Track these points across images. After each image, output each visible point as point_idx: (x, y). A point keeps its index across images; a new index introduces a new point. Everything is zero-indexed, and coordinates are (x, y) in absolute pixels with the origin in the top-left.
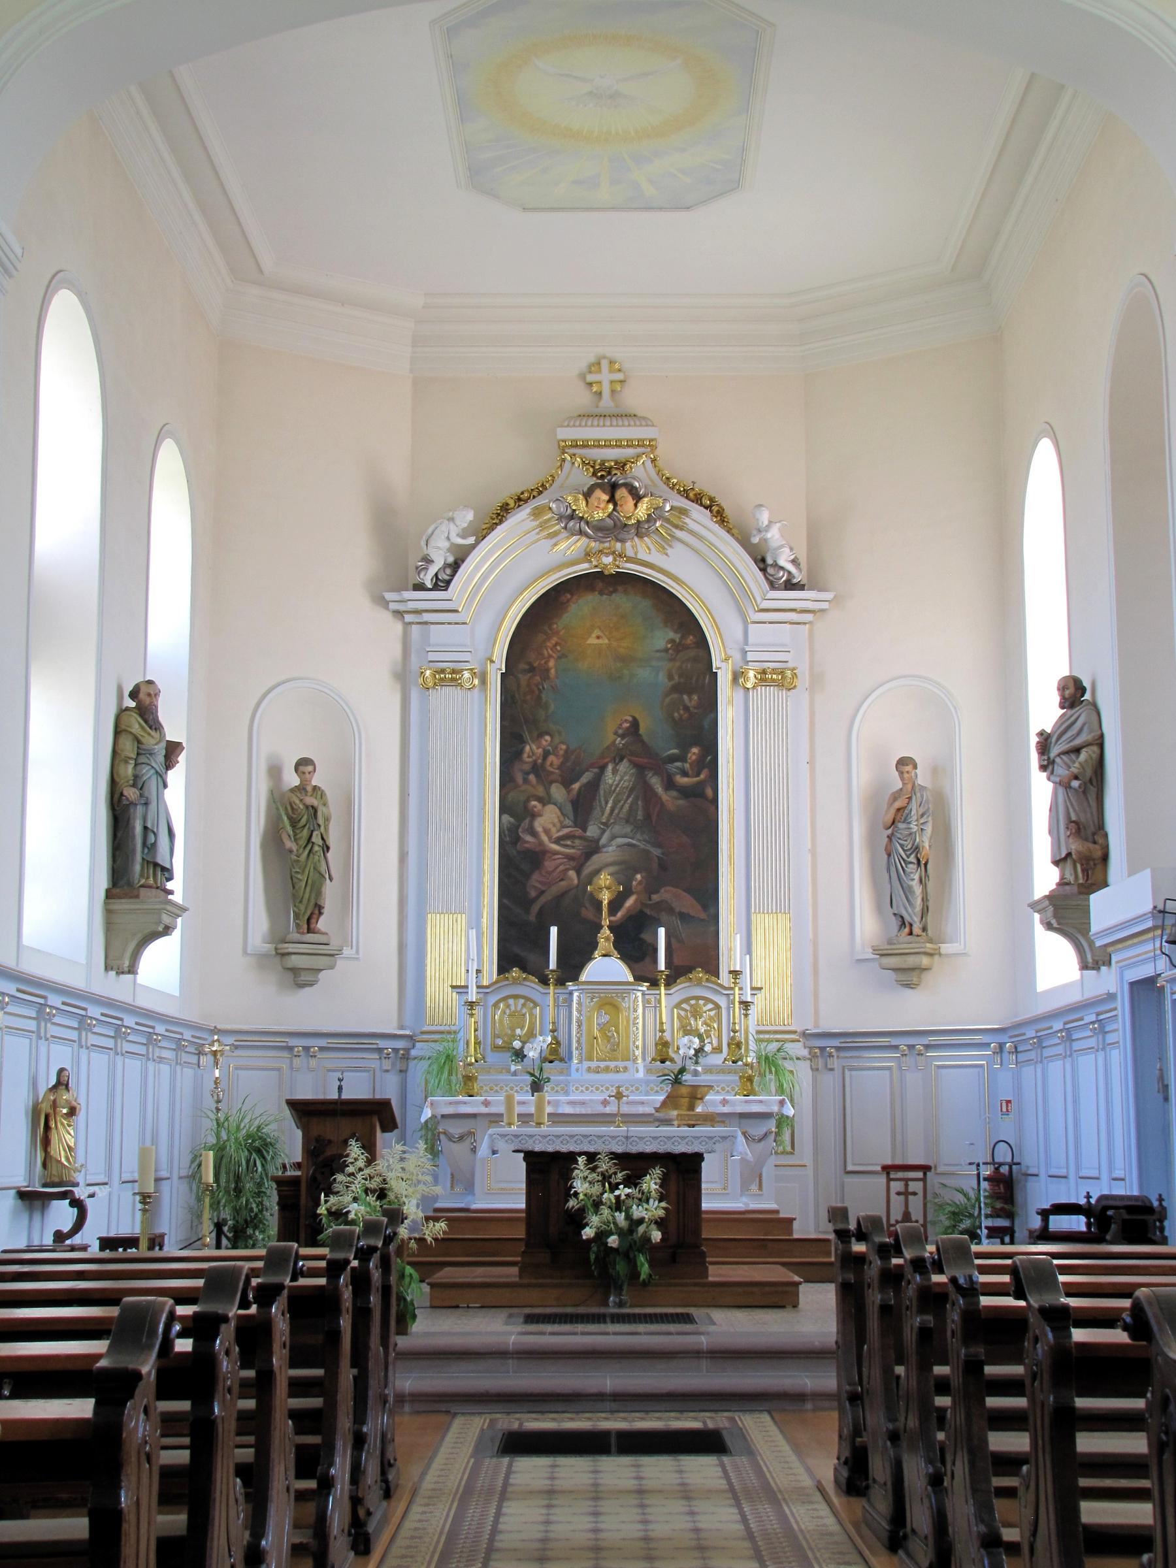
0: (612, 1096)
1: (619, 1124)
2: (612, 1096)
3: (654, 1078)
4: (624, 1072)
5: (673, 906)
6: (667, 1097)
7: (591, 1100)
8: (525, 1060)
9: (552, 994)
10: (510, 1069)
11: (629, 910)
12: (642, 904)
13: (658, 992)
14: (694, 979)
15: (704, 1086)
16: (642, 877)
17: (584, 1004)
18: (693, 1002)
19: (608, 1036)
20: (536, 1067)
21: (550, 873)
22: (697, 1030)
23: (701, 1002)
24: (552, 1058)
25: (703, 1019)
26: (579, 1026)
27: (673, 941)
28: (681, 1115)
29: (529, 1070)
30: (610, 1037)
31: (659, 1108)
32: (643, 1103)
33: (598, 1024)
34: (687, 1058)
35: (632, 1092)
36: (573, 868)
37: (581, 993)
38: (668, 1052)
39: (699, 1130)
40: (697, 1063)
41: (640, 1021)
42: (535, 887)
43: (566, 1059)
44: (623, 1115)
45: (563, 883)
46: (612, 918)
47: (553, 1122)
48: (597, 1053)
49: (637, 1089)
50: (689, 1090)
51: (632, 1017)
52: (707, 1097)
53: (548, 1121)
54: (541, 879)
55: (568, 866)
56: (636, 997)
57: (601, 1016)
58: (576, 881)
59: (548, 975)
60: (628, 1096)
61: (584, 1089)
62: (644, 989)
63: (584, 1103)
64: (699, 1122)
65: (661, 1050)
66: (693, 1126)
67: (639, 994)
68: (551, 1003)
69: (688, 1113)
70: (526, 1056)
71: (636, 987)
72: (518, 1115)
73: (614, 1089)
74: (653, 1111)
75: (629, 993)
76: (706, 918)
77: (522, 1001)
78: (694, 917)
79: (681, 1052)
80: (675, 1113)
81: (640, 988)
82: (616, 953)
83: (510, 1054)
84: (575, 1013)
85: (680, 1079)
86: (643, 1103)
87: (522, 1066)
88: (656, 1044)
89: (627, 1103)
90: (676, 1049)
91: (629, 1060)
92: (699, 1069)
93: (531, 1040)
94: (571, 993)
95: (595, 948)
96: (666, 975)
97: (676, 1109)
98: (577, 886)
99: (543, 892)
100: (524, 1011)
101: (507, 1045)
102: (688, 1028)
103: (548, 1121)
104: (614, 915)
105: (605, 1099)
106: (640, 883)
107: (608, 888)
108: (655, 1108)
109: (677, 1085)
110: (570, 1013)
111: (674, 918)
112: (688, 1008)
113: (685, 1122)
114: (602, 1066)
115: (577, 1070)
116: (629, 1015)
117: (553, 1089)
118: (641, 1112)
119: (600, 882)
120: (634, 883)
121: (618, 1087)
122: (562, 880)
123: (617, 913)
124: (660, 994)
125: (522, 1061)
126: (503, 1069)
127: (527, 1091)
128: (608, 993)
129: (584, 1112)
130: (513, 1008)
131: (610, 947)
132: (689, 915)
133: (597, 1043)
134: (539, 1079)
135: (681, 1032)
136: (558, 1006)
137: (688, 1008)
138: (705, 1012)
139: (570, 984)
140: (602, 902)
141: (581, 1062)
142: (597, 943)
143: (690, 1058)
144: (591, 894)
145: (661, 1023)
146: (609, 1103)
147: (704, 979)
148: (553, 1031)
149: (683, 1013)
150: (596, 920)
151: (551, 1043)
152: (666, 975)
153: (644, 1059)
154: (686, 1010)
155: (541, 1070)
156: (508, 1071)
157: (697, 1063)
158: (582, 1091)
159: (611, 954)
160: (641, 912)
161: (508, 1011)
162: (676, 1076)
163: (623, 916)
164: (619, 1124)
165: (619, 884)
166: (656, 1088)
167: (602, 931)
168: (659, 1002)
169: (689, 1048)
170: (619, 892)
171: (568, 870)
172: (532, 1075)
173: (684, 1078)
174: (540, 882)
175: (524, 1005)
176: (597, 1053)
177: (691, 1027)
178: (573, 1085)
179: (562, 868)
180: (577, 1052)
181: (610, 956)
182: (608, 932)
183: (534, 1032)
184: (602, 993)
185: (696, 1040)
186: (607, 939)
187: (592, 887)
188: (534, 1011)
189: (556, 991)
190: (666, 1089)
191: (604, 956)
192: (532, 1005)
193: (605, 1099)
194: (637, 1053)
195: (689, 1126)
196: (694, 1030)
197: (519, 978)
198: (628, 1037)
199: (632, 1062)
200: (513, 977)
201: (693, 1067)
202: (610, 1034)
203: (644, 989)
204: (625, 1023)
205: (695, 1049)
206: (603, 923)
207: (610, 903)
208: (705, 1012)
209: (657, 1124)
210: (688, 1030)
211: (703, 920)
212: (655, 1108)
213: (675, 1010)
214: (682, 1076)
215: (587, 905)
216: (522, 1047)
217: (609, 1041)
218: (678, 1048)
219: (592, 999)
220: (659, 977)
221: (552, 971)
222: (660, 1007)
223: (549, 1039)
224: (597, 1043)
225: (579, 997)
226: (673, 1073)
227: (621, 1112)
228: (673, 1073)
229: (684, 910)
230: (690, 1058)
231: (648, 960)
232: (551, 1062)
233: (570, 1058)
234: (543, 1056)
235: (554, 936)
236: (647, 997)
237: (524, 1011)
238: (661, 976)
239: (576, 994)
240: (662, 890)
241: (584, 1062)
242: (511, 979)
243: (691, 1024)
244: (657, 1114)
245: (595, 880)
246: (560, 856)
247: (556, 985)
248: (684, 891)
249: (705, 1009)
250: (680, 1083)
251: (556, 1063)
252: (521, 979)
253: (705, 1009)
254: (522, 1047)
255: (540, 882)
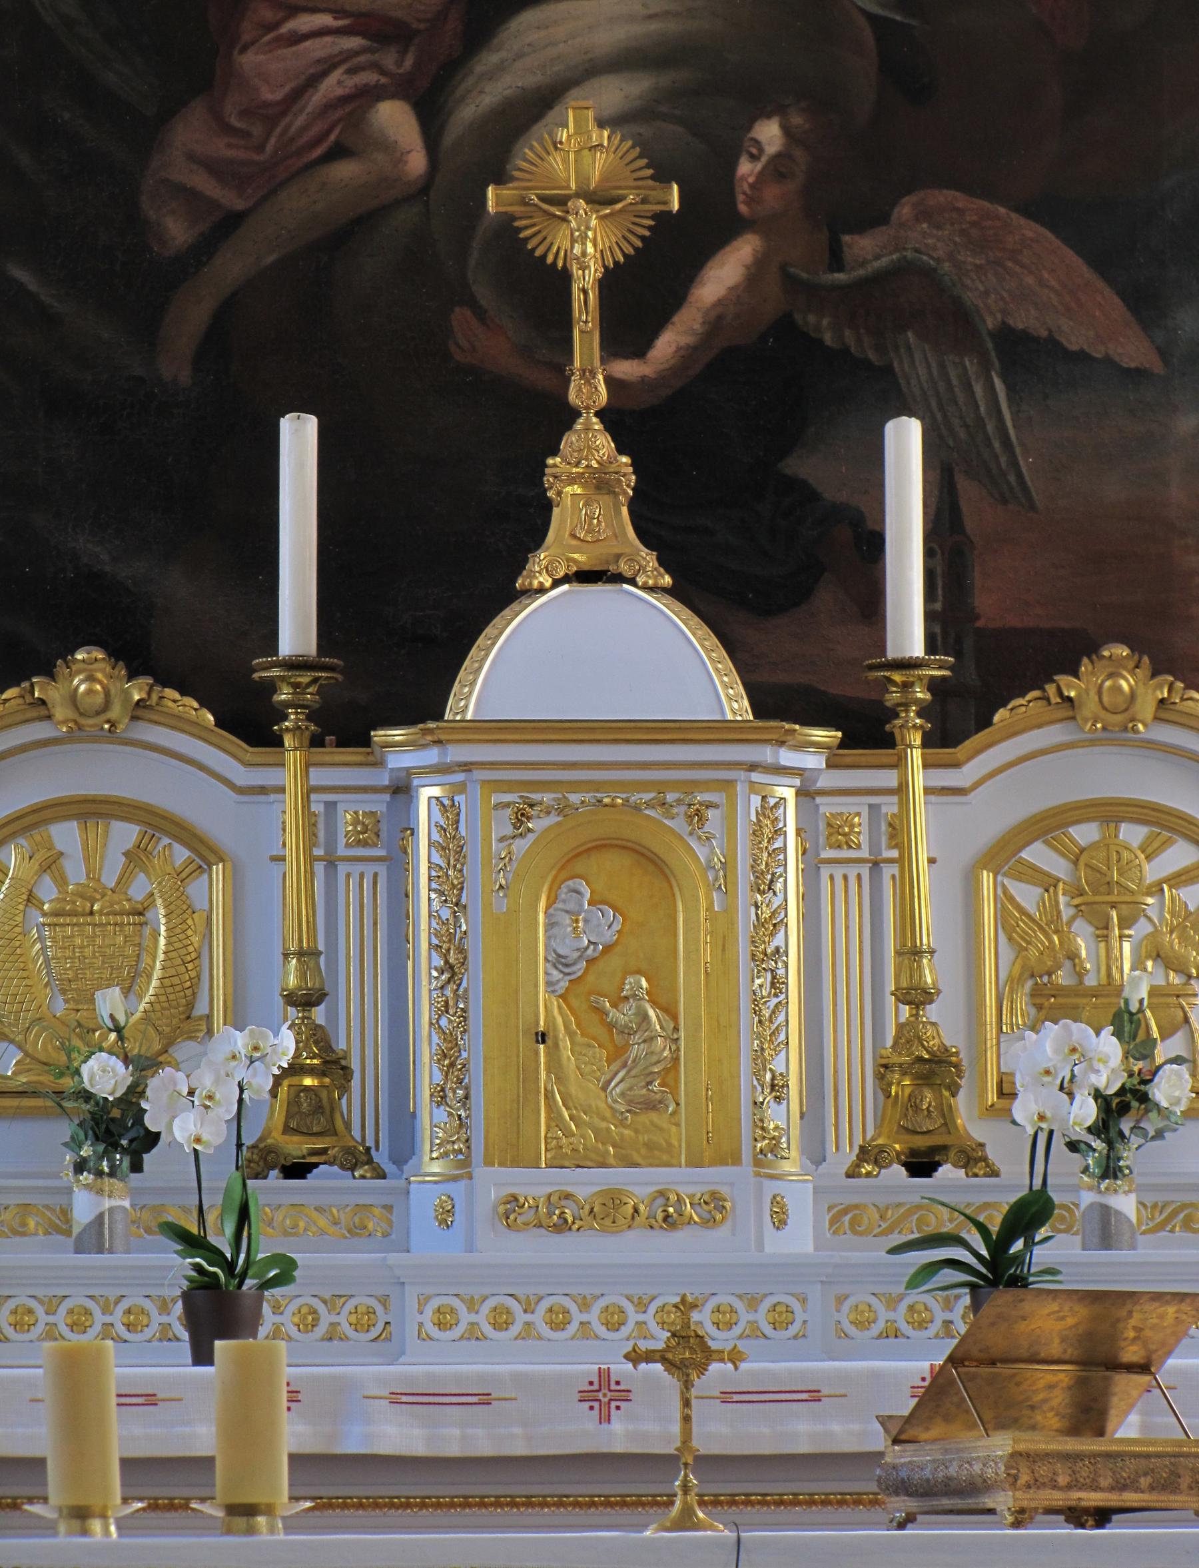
0: (649, 1357)
1: (687, 1511)
2: (649, 1357)
3: (873, 1253)
4: (709, 1222)
5: (970, 297)
6: (954, 1360)
7: (518, 1378)
8: (149, 1159)
9: (291, 799)
10: (66, 1213)
11: (716, 324)
12: (790, 282)
13: (889, 778)
14: (1090, 706)
15: (1157, 1297)
16: (786, 129)
17: (474, 853)
18: (1085, 833)
19: (611, 1026)
20: (213, 1202)
21: (273, 114)
22: (1111, 988)
23: (1132, 834)
24: (297, 1147)
25: (1141, 929)
26: (452, 972)
27: (969, 491)
28: (1031, 1458)
29: (174, 1216)
30: (627, 1032)
31: (909, 1420)
32: (815, 1396)
33: (559, 961)
34: (1058, 1144)
35: (755, 1332)
36: (401, 89)
37: (461, 788)
38: (947, 1116)
39: (912, 1535)
40: (1110, 1170)
41: (792, 938)
42: (190, 196)
43: (381, 1158)
44: (709, 1463)
45: (345, 171)
46: (627, 369)
47: (154, 1506)
48: (555, 1119)
49: (781, 1318)
50: (1075, 1317)
51: (745, 918)
52: (1171, 1362)
53: (294, 1498)
54: (221, 148)
55: (369, 78)
56: (770, 809)
57: (574, 914)
58: (417, 162)
59: (270, 687)
60: (735, 1357)
61: (482, 1318)
62: (813, 761)
63: (485, 1400)
64: (1131, 1498)
65: (913, 1104)
66: (1102, 1517)
67: (787, 792)
68: (292, 841)
69: (1072, 1445)
70: (152, 1139)
71: (767, 754)
72: (293, 1458)
73: (649, 1317)
74: (877, 1440)
75: (728, 784)
76: (1156, 366)
77: (125, 834)
78: (1082, 357)
79: (1024, 1110)
80: (1001, 1444)
81: (787, 757)
82: (649, 559)
83: (65, 1129)
84: (424, 898)
85: (1018, 1259)
86: (815, 1396)
87: (134, 1193)
88: (884, 1069)
89: (727, 1397)
90: (992, 1097)
91: (736, 1160)
92: (1126, 1204)
93: (183, 1050)
94: (402, 790)
95: (536, 535)
96: (934, 686)
97: (1002, 1426)
98: (426, 187)
99: (230, 223)
100: (140, 888)
101: (47, 1080)
102: (1062, 978)
103: (294, 1498)
104: (639, 352)
105: (604, 1376)
106: (778, 168)
107: (598, 199)
108: (884, 1421)
109: (1002, 1299)
110: (400, 897)
111: (970, 364)
112: (1057, 866)
113: (1058, 1498)
114: (582, 1193)
115: (445, 1216)
116: (729, 910)
117: (309, 1319)
118: (804, 1448)
119: (556, 161)
120: (746, 168)
121: (686, 1306)
122: (339, 152)
123: (649, 343)
124: (901, 790)
125: (137, 1167)
126: (25, 1209)
127: (166, 1335)
128: (575, 786)
129: (485, 1448)
130: (76, 872)
131: (618, 535)
132: (1052, 347)
133: (555, 1065)
134: (230, 1267)
135: (1022, 1002)
136: (331, 863)
137: (1057, 866)
138: (1156, 889)
139: (397, 734)
140: (565, 277)
141: (463, 1166)
142: (546, 507)
143: (1073, 1146)
144: (507, 227)
145: (912, 953)
146: (625, 1396)
147: (1146, 707)
148: (305, 1000)
149: (1027, 896)
150: (541, 379)
151: (295, 1069)
152: (934, 686)
153: (816, 1156)
154: (1049, 883)
155: (244, 1215)
156: (61, 1222)
157: (1110, 1170)
158: (473, 1334)
159: (625, 569)
160: (785, 326)
161: (48, 892)
162: (998, 1246)
163: (687, 356)
164: (687, 1511)
165: (663, 176)
166: (883, 1314)
167: (569, 441)
168: (898, 832)
169: (1068, 1090)
170: (663, 218)
171: (368, 96)
172: (192, 1242)
173: (1041, 1256)
174: (216, 169)
175: (136, 857)
176: (555, 1119)
177: (1080, 974)
178: (423, 1301)
179: (333, 85)
180: (441, 1114)
181: (618, 578)
182: (604, 444)
183: (201, 1009)
184: (575, 786)
185: (1109, 1046)
186: (601, 483)
187: (508, 192)
188: (196, 888)
189: (318, 777)
190: (940, 1316)
191: (585, 577)
192: (181, 854)
193: (604, 1376)
194: (775, 1116)
195: (1076, 1516)
196: (1095, 993)
197: (107, 706)
198: (724, 1029)
199: (747, 1167)
200: (73, 698)
201: (1088, 1198)
202: (622, 1016)
203: (813, 761)
204: (707, 955)
205: (1097, 1095)
206: (572, 397)
207: (611, 281)
208: (1156, 889)
209: (900, 1505)
210: (1059, 992)
211: (1137, 375)
212: (884, 1421)
213: (987, 878)
214: (1030, 1244)
215: (484, 294)
216: (136, 1091)
217: (618, 1053)
218: (1006, 1092)
219: (521, 818)
220: (894, 697)
221: (296, 665)
222: (904, 861)
223: (285, 1044)
224: (555, 1065)
225: (447, 807)
226: (982, 1229)
227: (703, 1444)
228: (982, 1229)
229: (1024, 319)
230: (1073, 1146)
231: (826, 597)
232: (297, 1170)
233: (404, 1151)
234: (248, 1141)
235: (300, 466)
236: (827, 807)
237: (140, 888)
238: (907, 686)
239: (427, 793)
240: (904, 210)
241: (481, 1172)
242: (59, 713)
243: (1073, 956)
244: (898, 1456)
245: (526, 154)
246: (325, 20)
247: (316, 742)
248: (1026, 210)
249: (1152, 871)
250: (1019, 1282)
251: (325, 1178)
252: (115, 712)
253: (1152, 871)
254: (136, 1091)
255: (216, 169)
